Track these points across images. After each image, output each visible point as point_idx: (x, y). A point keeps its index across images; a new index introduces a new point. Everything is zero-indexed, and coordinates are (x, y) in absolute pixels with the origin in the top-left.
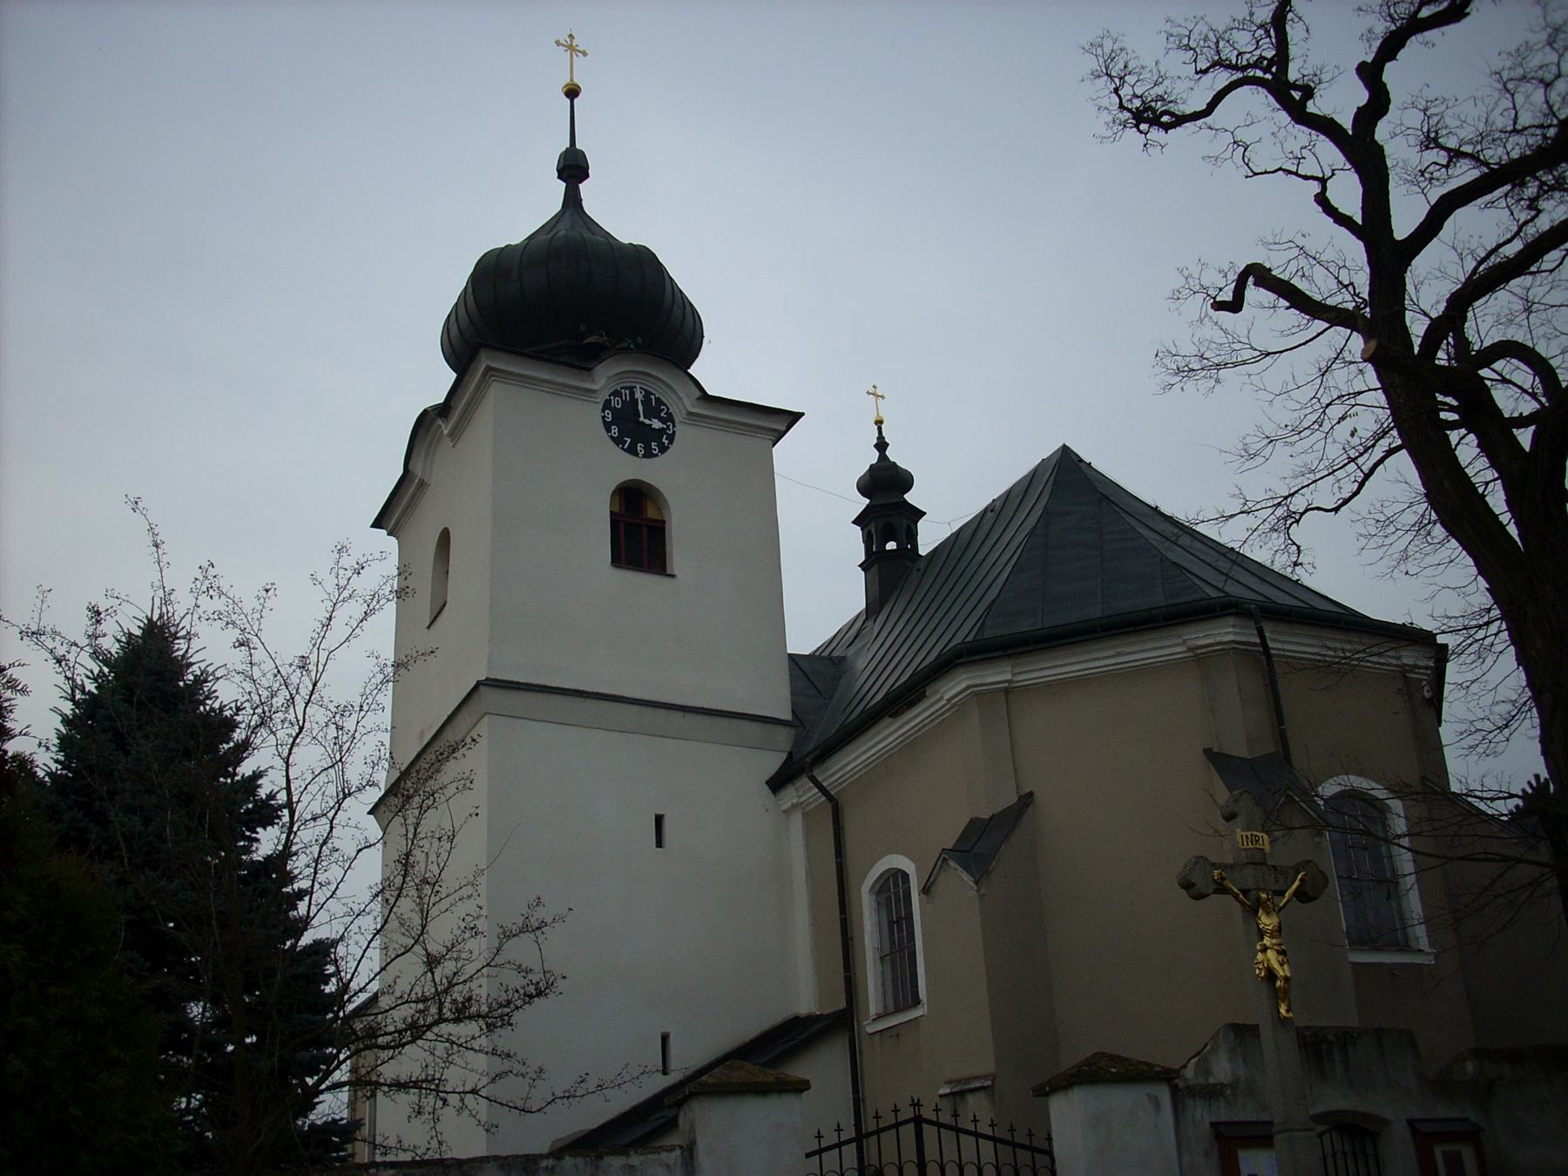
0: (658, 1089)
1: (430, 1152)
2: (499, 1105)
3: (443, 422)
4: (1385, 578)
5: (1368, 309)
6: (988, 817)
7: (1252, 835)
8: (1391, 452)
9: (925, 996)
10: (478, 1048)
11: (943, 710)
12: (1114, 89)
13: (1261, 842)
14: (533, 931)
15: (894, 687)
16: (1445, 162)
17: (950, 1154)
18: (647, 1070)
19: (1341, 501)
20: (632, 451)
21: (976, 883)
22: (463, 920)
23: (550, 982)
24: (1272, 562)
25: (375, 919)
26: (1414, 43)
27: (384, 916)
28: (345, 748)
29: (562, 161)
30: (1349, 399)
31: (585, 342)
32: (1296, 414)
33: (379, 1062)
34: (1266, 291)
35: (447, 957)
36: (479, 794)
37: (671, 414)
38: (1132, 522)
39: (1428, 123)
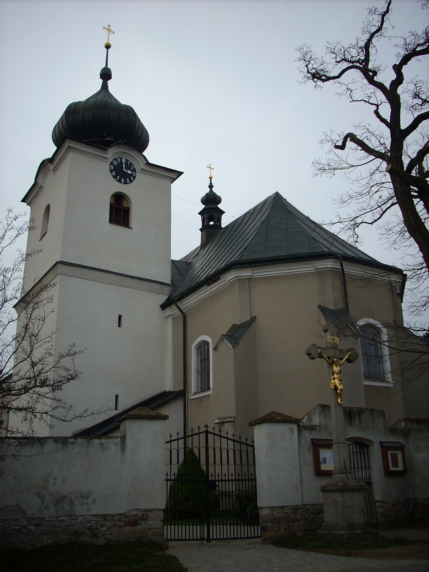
0: (114, 415)
1: (29, 434)
2: (55, 418)
3: (51, 165)
5: (389, 153)
6: (239, 324)
7: (333, 338)
8: (393, 205)
10: (48, 397)
12: (306, 65)
13: (336, 340)
14: (72, 355)
15: (209, 275)
16: (421, 104)
17: (217, 445)
18: (110, 408)
19: (374, 220)
20: (120, 181)
21: (233, 348)
22: (46, 350)
23: (77, 375)
24: (348, 240)
25: (14, 347)
26: (414, 59)
27: (17, 347)
28: (6, 284)
29: (102, 71)
30: (380, 185)
31: (105, 139)
32: (361, 189)
33: (12, 400)
34: (354, 143)
35: (39, 363)
36: (54, 305)
37: (135, 169)
38: (299, 222)
39: (416, 89)
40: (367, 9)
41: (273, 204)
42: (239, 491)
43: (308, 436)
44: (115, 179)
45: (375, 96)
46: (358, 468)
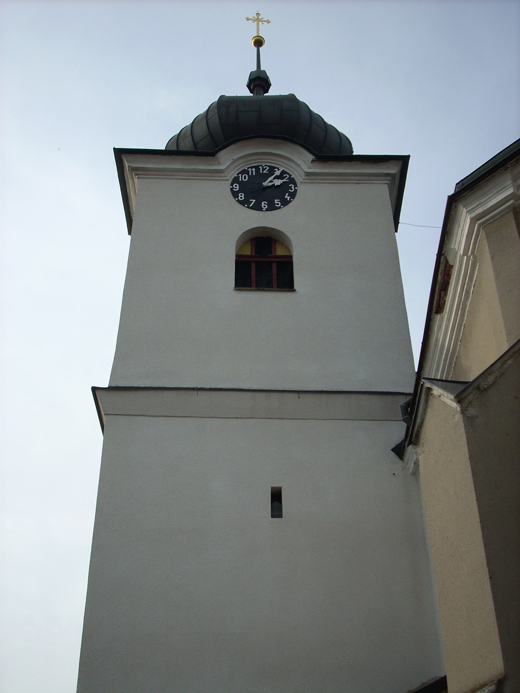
44: (244, 206)
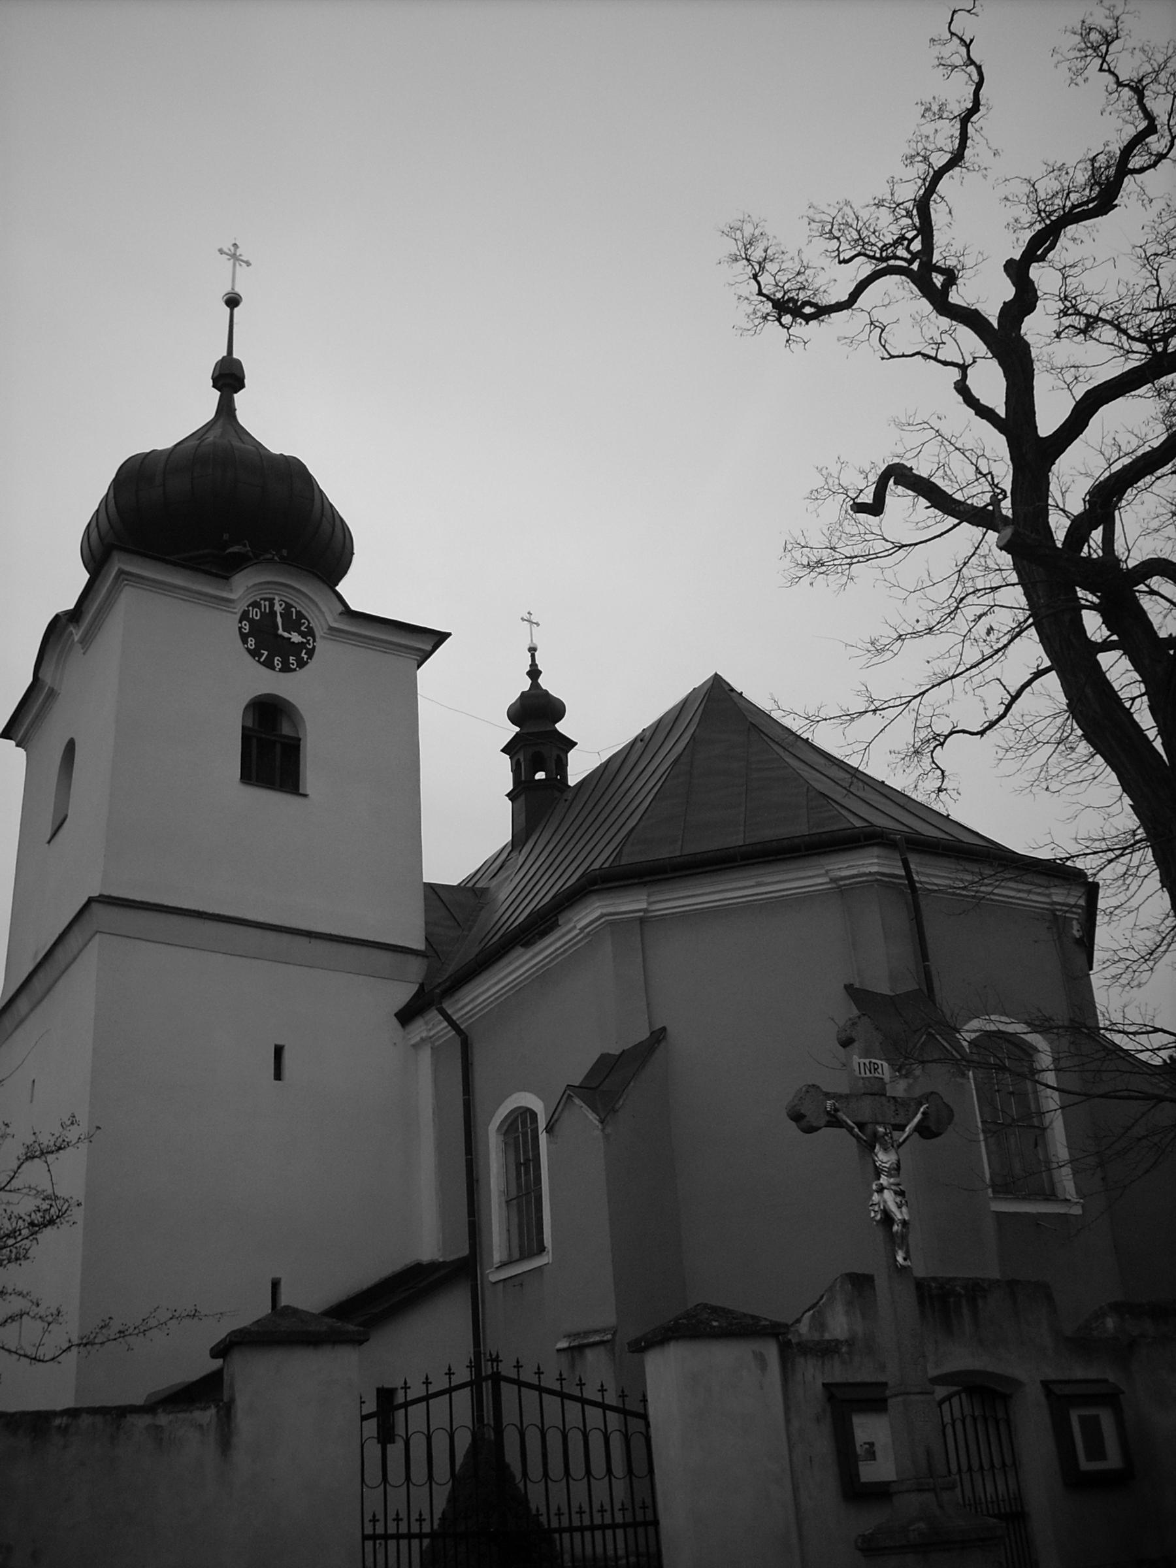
3: (74, 628)
4: (1023, 792)
6: (617, 1053)
7: (870, 1063)
9: (550, 1244)
11: (575, 940)
13: (880, 1070)
18: (177, 1314)
19: (987, 724)
20: (269, 664)
21: (602, 1122)
31: (228, 551)
37: (312, 628)
40: (917, 104)
41: (704, 710)
42: (638, 1555)
43: (814, 1377)
44: (254, 658)
45: (955, 341)
46: (981, 1467)
